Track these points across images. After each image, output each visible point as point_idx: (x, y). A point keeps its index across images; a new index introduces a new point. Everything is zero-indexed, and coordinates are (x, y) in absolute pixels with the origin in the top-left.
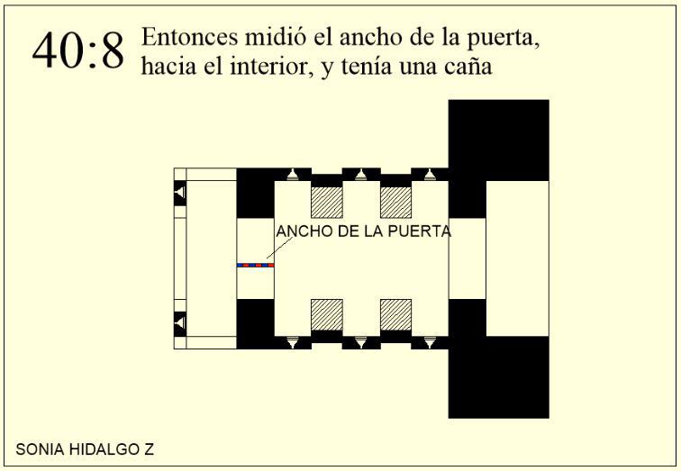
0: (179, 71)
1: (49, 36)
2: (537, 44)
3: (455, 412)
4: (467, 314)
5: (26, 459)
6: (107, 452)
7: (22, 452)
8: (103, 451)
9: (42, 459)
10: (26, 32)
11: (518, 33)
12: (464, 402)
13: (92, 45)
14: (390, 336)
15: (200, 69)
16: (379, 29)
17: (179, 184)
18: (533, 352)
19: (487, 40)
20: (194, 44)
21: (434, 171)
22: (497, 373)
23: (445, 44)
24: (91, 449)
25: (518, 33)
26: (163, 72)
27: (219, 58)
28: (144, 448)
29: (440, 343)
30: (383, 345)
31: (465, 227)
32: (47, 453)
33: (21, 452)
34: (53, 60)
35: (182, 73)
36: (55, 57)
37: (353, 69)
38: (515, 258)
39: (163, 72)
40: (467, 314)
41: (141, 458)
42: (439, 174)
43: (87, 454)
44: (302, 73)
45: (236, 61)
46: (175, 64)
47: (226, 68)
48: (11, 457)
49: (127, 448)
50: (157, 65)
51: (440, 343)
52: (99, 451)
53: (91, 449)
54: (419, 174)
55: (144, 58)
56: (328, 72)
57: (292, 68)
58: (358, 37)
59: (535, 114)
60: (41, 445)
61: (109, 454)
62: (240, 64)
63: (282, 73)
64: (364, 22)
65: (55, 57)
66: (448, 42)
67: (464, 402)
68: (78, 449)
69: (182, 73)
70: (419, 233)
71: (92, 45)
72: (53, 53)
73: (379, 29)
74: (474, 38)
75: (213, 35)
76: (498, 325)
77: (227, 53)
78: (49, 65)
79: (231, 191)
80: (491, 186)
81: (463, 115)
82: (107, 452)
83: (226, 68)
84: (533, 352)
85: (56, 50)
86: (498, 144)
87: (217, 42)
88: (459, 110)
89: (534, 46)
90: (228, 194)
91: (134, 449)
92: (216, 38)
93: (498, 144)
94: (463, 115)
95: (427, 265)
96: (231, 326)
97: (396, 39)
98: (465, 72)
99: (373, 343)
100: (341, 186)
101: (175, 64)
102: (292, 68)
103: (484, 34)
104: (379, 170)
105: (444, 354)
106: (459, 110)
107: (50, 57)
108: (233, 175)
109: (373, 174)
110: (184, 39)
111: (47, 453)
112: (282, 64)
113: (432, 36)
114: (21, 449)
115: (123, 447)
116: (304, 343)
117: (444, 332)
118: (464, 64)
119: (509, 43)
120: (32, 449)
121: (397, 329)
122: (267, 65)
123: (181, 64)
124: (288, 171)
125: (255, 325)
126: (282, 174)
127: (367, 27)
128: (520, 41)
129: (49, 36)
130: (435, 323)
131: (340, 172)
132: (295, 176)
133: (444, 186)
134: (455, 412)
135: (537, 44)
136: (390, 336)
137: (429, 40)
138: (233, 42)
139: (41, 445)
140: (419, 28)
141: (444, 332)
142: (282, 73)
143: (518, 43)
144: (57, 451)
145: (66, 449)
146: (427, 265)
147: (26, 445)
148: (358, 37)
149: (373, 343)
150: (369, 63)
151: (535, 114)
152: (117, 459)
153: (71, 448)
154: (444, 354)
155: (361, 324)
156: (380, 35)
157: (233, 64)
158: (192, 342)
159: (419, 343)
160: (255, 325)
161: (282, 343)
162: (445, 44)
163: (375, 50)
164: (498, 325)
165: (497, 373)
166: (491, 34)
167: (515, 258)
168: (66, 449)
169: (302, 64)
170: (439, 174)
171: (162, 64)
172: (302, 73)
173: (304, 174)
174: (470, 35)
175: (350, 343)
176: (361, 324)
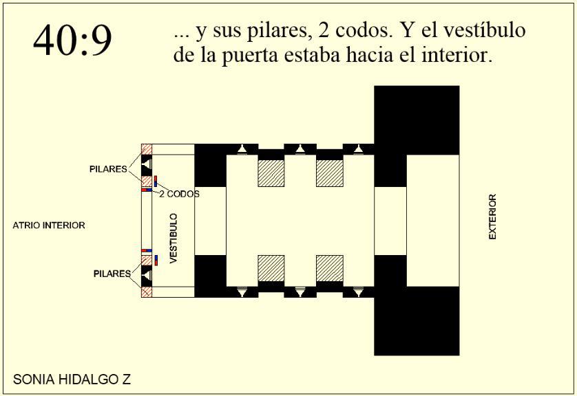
0: (378, 59)
1: (48, 28)
2: (310, 36)
3: (456, 352)
4: (390, 269)
5: (22, 388)
6: (90, 382)
7: (18, 381)
8: (88, 380)
9: (36, 388)
10: (25, 25)
11: (265, 51)
12: (389, 341)
13: (84, 36)
14: (325, 287)
15: (396, 57)
16: (322, 48)
17: (146, 158)
18: (447, 299)
19: (239, 58)
20: (262, 36)
21: (362, 146)
22: (415, 318)
23: (204, 61)
24: (77, 379)
25: (265, 51)
26: (365, 61)
27: (412, 47)
28: (122, 379)
29: (367, 292)
30: (318, 294)
31: (391, 193)
32: (40, 383)
33: (18, 381)
34: (51, 48)
35: (381, 61)
36: (52, 45)
37: (450, 58)
38: (430, 221)
39: (365, 61)
40: (390, 269)
41: (119, 387)
42: (367, 149)
43: (74, 383)
44: (483, 61)
45: (427, 50)
46: (375, 53)
47: (419, 56)
48: (11, 387)
49: (108, 378)
50: (360, 54)
51: (367, 292)
52: (84, 380)
53: (77, 379)
54: (349, 149)
55: (349, 48)
56: (202, 35)
57: (474, 57)
58: (503, 33)
59: (448, 98)
60: (34, 375)
61: (93, 383)
62: (430, 53)
63: (466, 61)
64: (353, 17)
65: (52, 45)
66: (206, 59)
67: (389, 341)
68: (66, 379)
69: (381, 61)
70: (494, 217)
71: (84, 36)
72: (51, 42)
73: (322, 48)
74: (228, 56)
75: (343, 28)
76: (416, 277)
77: (298, 44)
78: (48, 53)
79: (190, 162)
80: (411, 159)
81: (388, 100)
82: (90, 382)
83: (419, 56)
84: (447, 299)
85: (53, 40)
86: (415, 124)
87: (346, 34)
88: (384, 95)
89: (307, 37)
90: (187, 167)
91: (113, 379)
92: (345, 31)
93: (415, 124)
94: (388, 100)
95: (351, 221)
96: (190, 279)
97: (520, 32)
98: (278, 36)
99: (310, 292)
100: (342, 159)
101: (375, 53)
102: (474, 57)
103: (500, 28)
104: (315, 145)
105: (370, 302)
106: (384, 95)
107: (48, 46)
108: (192, 150)
109: (310, 149)
110: (374, 32)
111: (40, 383)
112: (466, 53)
113: (193, 54)
114: (18, 379)
115: (105, 377)
116: (252, 292)
117: (371, 283)
118: (278, 28)
119: (257, 61)
120: (27, 379)
121: (146, 264)
122: (453, 54)
123: (381, 53)
124: (238, 146)
125: (211, 277)
126: (233, 149)
127: (469, 22)
128: (268, 59)
129: (48, 28)
130: (362, 275)
131: (341, 148)
132: (303, 151)
133: (370, 159)
134: (456, 352)
135: (310, 36)
136: (325, 287)
137: (189, 58)
138: (237, 35)
139: (34, 375)
140: (182, 48)
141: (371, 283)
142: (466, 61)
143: (265, 61)
144: (48, 380)
145: (56, 379)
146: (351, 221)
147: (22, 376)
148: (503, 33)
149: (310, 292)
150: (354, 52)
151: (448, 98)
152: (99, 388)
153: (60, 379)
154: (370, 302)
155: (300, 277)
156: (322, 53)
157: (424, 53)
158: (156, 292)
159: (349, 292)
160: (211, 277)
161: (233, 293)
162: (204, 61)
163: (379, 40)
164: (416, 277)
165: (415, 318)
166: (242, 53)
167: (430, 221)
168: (56, 379)
169: (483, 53)
170: (367, 149)
171: (364, 53)
172: (483, 61)
173: (252, 149)
174: (225, 53)
175: (291, 292)
176: (300, 277)
